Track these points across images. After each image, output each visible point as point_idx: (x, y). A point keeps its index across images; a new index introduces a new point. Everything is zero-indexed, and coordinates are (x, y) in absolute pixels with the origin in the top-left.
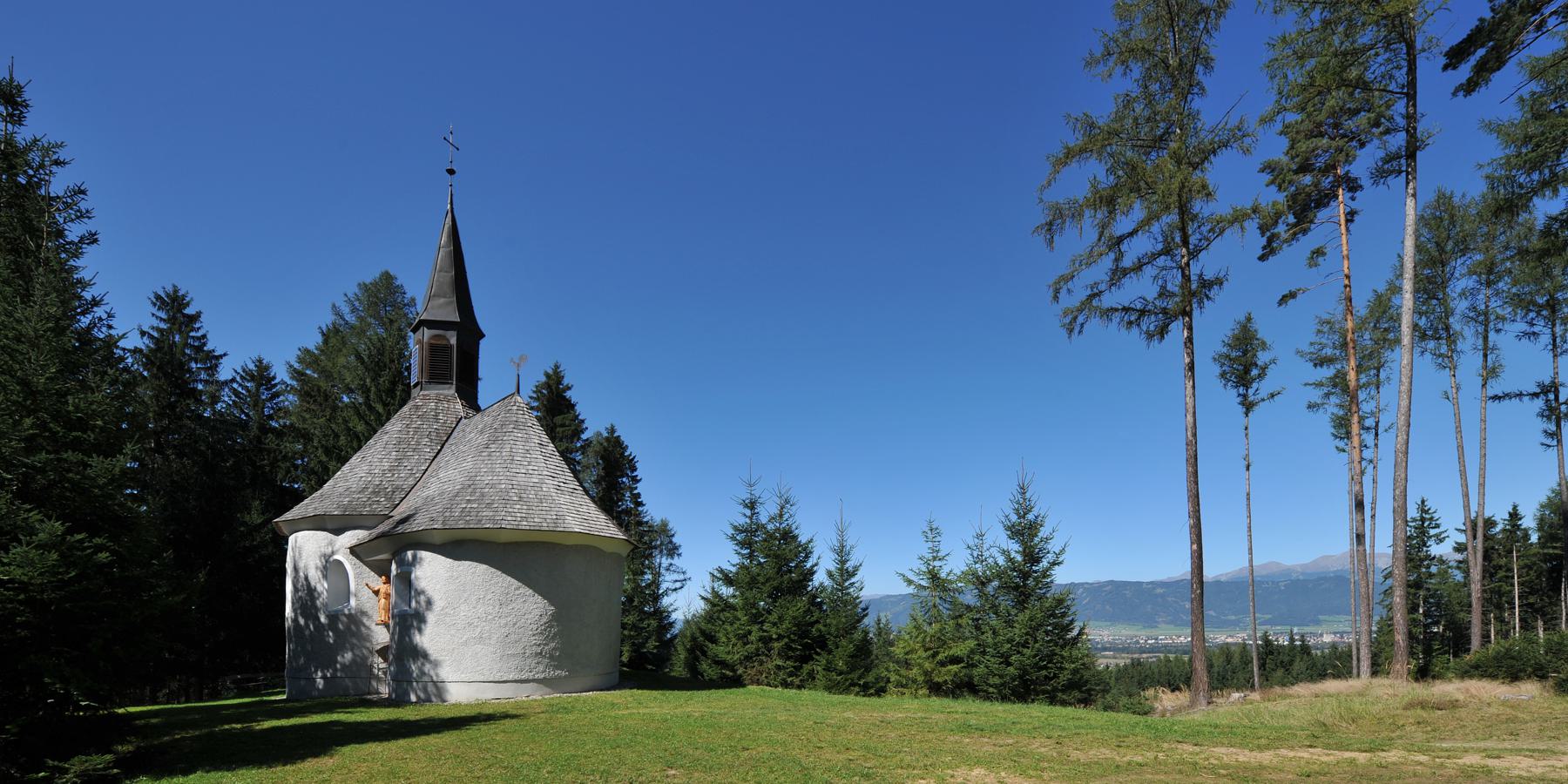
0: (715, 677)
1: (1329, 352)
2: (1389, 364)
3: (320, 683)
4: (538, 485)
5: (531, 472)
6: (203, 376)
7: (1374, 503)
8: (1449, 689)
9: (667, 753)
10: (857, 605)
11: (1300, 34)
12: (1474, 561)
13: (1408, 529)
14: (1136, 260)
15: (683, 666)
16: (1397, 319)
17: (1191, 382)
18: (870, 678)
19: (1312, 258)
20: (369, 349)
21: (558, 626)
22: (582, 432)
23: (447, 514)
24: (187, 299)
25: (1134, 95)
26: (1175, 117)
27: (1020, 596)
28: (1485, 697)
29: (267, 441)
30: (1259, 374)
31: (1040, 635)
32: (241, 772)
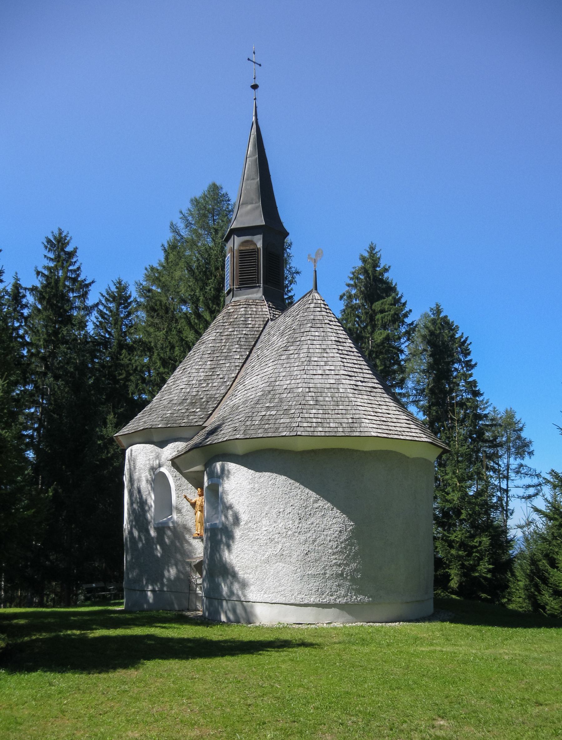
4: (335, 386)
5: (327, 372)
22: (406, 316)
24: (68, 239)
29: (122, 357)
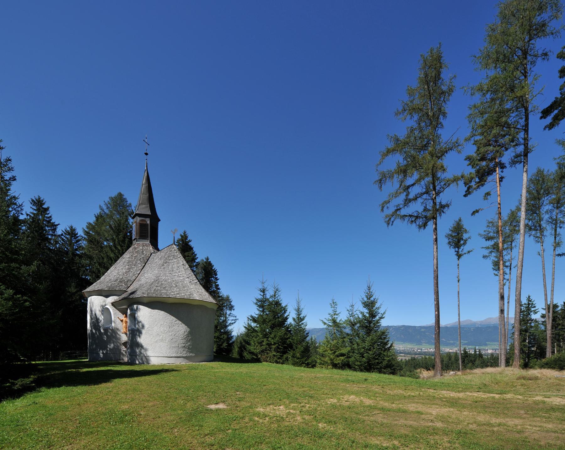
0: (249, 359)
1: (491, 234)
2: (516, 240)
3: (101, 355)
4: (183, 281)
5: (180, 275)
6: (51, 233)
7: (509, 297)
8: (535, 372)
9: (235, 386)
10: (304, 332)
11: (482, 103)
12: (548, 321)
13: (522, 308)
14: (414, 196)
15: (237, 353)
16: (519, 222)
17: (436, 246)
18: (310, 361)
19: (485, 196)
20: (115, 224)
21: (191, 336)
22: (196, 259)
23: (149, 291)
24: (44, 202)
25: (414, 127)
26: (431, 137)
27: (368, 330)
28: (549, 376)
30: (464, 243)
31: (376, 346)
32: (79, 387)
